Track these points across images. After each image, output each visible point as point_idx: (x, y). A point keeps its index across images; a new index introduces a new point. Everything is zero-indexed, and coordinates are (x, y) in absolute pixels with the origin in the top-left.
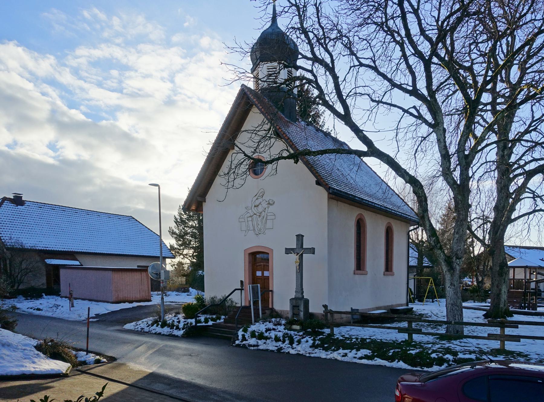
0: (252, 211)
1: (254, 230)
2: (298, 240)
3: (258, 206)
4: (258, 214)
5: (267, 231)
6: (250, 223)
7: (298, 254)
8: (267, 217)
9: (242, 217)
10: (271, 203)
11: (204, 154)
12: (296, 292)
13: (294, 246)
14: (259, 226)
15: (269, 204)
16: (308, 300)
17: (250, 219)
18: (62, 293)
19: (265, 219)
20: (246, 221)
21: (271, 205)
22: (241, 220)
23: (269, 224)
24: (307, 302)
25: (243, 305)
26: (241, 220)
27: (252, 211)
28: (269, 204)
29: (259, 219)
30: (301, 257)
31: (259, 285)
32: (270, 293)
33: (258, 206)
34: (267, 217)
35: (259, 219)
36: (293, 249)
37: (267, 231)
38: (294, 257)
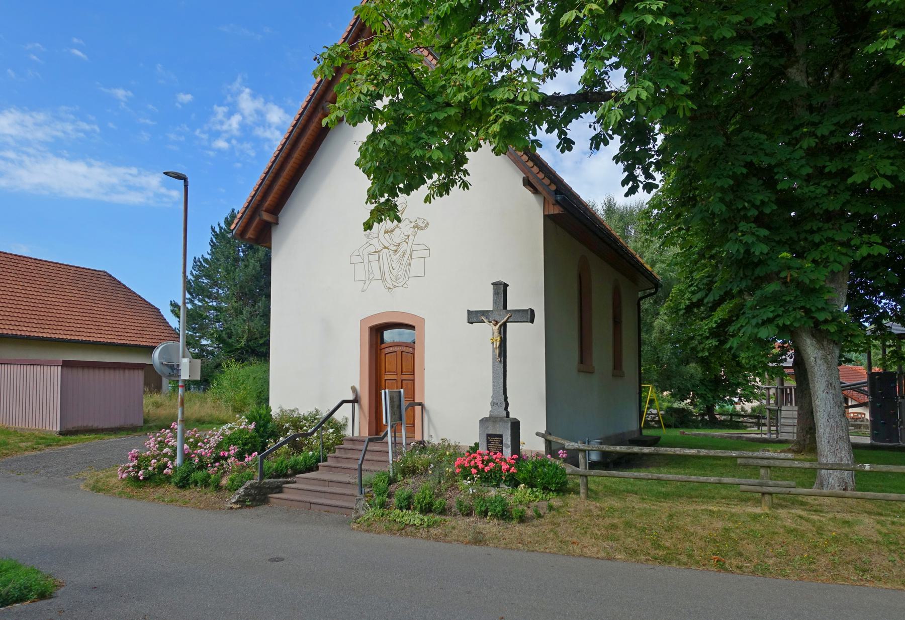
0: (379, 241)
1: (383, 279)
2: (496, 292)
3: (392, 231)
4: (392, 247)
5: (411, 282)
6: (375, 265)
7: (497, 323)
8: (411, 254)
9: (357, 253)
10: (421, 224)
11: (282, 131)
12: (493, 404)
13: (490, 307)
14: (395, 273)
15: (416, 226)
16: (519, 422)
17: (376, 257)
18: (257, 323)
19: (406, 256)
20: (366, 261)
21: (421, 228)
22: (354, 260)
23: (417, 267)
24: (515, 426)
25: (356, 434)
26: (354, 260)
27: (379, 241)
28: (416, 226)
29: (394, 258)
30: (503, 330)
31: (402, 390)
32: (418, 409)
33: (392, 231)
34: (411, 254)
35: (394, 258)
36: (484, 313)
37: (411, 282)
38: (487, 331)
